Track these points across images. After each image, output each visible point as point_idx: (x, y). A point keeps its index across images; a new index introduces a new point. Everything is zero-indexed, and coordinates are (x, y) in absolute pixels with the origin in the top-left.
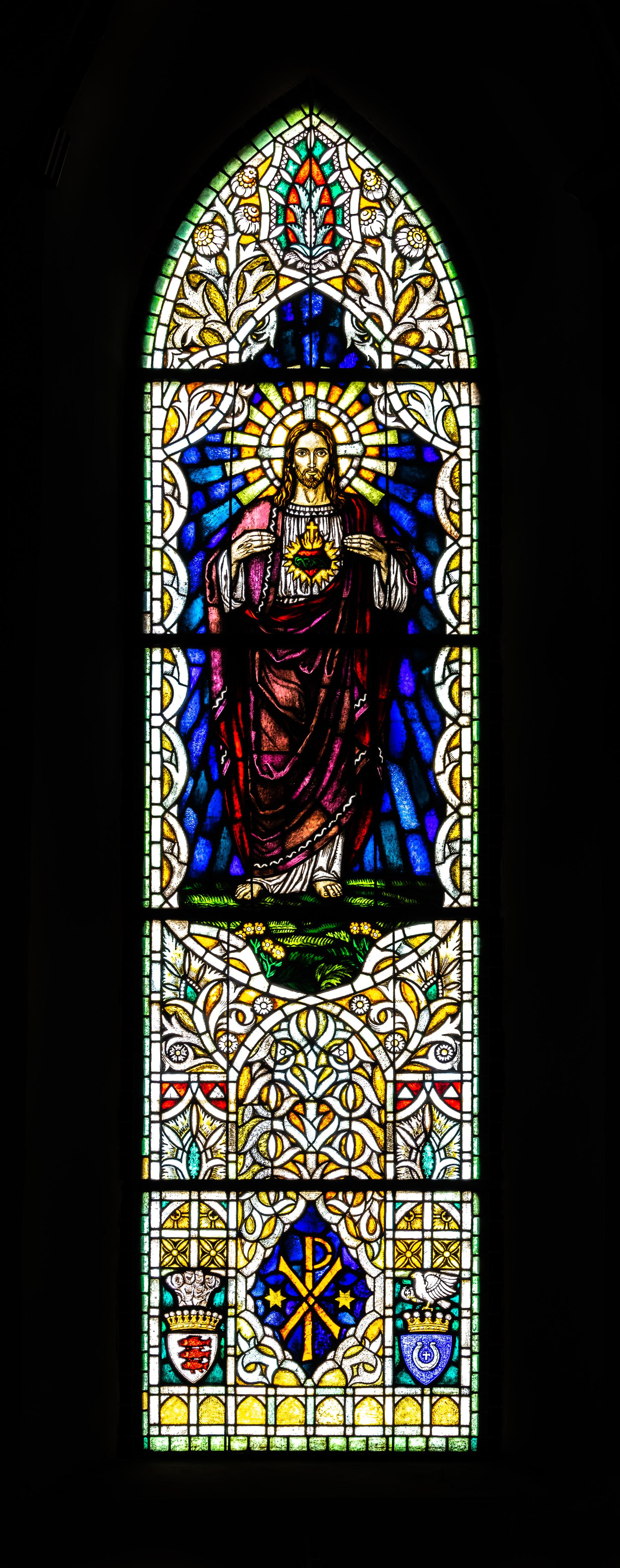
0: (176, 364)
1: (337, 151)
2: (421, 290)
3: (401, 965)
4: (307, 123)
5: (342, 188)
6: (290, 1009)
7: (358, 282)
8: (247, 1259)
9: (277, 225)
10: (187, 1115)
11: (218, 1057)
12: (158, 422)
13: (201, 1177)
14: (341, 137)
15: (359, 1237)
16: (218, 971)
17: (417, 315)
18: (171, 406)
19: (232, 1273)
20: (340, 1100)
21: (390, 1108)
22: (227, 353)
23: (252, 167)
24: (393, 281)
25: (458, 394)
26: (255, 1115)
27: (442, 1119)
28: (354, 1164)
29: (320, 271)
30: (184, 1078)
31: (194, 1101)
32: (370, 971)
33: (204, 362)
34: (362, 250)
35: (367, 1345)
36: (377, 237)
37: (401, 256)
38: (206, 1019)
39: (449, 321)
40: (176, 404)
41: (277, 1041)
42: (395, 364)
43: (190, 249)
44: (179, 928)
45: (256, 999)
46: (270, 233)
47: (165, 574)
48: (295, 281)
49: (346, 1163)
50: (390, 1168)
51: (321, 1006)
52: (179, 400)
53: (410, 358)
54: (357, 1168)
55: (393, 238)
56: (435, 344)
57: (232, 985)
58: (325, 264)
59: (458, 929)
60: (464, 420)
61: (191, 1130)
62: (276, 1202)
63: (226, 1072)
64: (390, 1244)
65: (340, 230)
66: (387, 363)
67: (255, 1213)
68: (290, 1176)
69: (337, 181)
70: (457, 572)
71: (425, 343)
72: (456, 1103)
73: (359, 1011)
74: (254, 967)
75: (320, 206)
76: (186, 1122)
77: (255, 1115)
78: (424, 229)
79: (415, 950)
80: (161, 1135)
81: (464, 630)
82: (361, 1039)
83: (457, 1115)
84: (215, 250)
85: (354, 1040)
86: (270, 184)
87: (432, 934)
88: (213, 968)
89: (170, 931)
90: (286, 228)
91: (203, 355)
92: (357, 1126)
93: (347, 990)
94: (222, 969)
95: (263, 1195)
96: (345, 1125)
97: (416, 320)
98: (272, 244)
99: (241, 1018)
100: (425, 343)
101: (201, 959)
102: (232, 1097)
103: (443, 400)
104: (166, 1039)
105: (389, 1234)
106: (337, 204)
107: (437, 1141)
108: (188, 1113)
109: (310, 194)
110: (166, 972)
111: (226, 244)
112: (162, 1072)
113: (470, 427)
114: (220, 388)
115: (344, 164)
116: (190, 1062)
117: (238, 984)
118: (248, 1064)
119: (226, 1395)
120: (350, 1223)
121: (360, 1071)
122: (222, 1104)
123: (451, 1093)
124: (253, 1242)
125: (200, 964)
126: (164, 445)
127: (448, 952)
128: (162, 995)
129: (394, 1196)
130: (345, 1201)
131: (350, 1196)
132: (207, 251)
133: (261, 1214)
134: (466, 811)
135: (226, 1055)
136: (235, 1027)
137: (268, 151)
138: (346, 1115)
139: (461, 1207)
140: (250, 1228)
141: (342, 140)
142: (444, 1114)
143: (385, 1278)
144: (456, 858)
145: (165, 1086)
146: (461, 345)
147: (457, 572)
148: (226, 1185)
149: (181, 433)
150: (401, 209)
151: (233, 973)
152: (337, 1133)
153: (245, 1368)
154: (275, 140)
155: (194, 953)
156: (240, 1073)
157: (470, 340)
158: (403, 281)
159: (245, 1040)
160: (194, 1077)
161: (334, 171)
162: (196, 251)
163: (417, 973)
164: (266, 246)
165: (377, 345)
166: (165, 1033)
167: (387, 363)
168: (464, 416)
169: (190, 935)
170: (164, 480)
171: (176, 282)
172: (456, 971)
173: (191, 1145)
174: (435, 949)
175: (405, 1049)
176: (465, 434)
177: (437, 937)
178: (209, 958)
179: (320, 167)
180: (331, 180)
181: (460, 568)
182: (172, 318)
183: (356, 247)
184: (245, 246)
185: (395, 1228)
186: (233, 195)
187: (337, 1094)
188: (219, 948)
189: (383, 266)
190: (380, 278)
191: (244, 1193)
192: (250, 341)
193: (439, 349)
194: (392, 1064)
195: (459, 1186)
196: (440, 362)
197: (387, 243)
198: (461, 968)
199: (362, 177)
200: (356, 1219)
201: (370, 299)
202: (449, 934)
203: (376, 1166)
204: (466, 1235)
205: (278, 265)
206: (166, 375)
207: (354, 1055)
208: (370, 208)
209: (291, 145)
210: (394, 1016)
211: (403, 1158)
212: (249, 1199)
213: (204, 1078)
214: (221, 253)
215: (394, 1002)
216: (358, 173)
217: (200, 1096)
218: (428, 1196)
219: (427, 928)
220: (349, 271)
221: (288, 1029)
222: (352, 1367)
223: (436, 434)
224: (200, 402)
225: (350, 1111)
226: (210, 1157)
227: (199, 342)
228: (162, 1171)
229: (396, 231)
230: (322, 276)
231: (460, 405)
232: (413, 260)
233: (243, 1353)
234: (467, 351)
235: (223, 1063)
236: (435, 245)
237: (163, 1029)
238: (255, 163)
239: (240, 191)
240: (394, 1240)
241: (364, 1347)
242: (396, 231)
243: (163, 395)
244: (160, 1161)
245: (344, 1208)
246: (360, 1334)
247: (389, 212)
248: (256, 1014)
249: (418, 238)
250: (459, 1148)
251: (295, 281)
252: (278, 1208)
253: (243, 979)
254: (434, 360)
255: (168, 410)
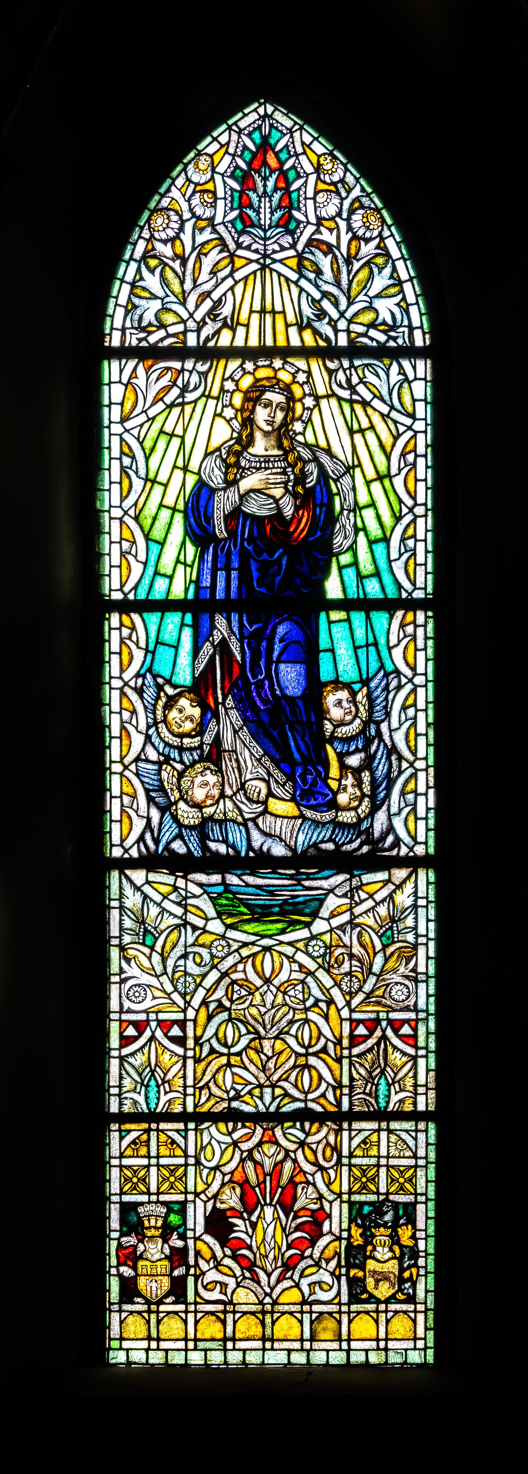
0: (134, 343)
1: (292, 137)
2: (376, 270)
3: (358, 910)
4: (261, 111)
5: (281, 132)
6: (245, 952)
7: (314, 263)
8: (206, 1183)
9: (232, 209)
10: (146, 1051)
11: (176, 997)
12: (117, 397)
13: (158, 1110)
14: (296, 123)
15: (316, 1164)
16: (175, 916)
17: (372, 293)
18: (129, 382)
19: (190, 1197)
20: (296, 1037)
21: (345, 1043)
22: (185, 333)
23: (206, 154)
24: (348, 262)
25: (414, 368)
26: (212, 1051)
27: (398, 1055)
28: (311, 1096)
29: (274, 252)
30: (143, 1017)
31: (153, 1038)
32: (326, 916)
33: (162, 340)
34: (318, 231)
35: (324, 1265)
36: (332, 219)
37: (355, 237)
38: (164, 960)
39: (404, 299)
40: (134, 381)
41: (233, 982)
42: (350, 341)
43: (146, 234)
44: (138, 876)
45: (212, 943)
46: (225, 216)
47: (123, 542)
48: (250, 261)
49: (302, 1096)
50: (345, 1101)
51: (276, 948)
52: (136, 377)
53: (365, 335)
54: (313, 1100)
55: (348, 220)
56: (390, 321)
57: (189, 928)
58: (280, 245)
59: (413, 879)
60: (419, 394)
61: (150, 1065)
62: (235, 1129)
63: (184, 1011)
64: (345, 1170)
65: (295, 213)
66: (343, 341)
67: (213, 1142)
68: (247, 1109)
69: (293, 167)
70: (413, 540)
71: (380, 320)
72: (412, 1040)
73: (316, 954)
74: (211, 912)
75: (276, 189)
76: (145, 1058)
77: (212, 1051)
78: (378, 210)
79: (371, 896)
80: (120, 1069)
81: (419, 594)
82: (316, 979)
83: (411, 1051)
84: (171, 233)
85: (309, 979)
86: (226, 172)
87: (389, 881)
88: (171, 914)
89: (128, 879)
90: (242, 212)
91: (162, 333)
92: (313, 1061)
93: (304, 933)
94: (180, 915)
95: (222, 1126)
96: (302, 1061)
97: (371, 298)
98: (226, 227)
99: (198, 960)
100: (380, 320)
101: (159, 905)
102: (190, 1033)
103: (399, 373)
104: (123, 981)
105: (345, 1161)
106: (293, 188)
107: (392, 1075)
108: (147, 1048)
109: (265, 179)
110: (125, 917)
111: (181, 229)
112: (121, 1012)
113: (425, 400)
114: (177, 365)
115: (299, 150)
116: (148, 1004)
117: (195, 928)
118: (204, 1003)
119: (186, 1312)
120: (308, 1152)
121: (316, 1010)
122: (181, 1041)
123: (406, 1030)
124: (211, 1169)
125: (158, 910)
126: (123, 420)
127: (403, 899)
128: (121, 940)
129: (350, 1125)
130: (303, 1129)
131: (307, 1125)
132: (163, 236)
133: (219, 1142)
134: (420, 765)
135: (183, 996)
136: (192, 968)
137: (224, 139)
138: (303, 1051)
139: (416, 1026)
140: (209, 1155)
141: (297, 127)
142: (398, 1050)
143: (342, 1202)
144: (412, 818)
145: (124, 1025)
146: (416, 323)
147: (413, 540)
148: (184, 1117)
149: (138, 410)
150: (356, 192)
151: (191, 918)
152: (295, 1067)
153: (205, 1287)
154: (230, 128)
155: (151, 900)
156: (197, 1011)
157: (424, 318)
158: (358, 260)
159: (202, 981)
160: (153, 1016)
161: (291, 157)
162: (152, 236)
163: (372, 919)
164: (221, 229)
165: (333, 324)
166: (123, 976)
167: (343, 341)
168: (419, 389)
169: (148, 882)
170: (122, 452)
171: (133, 266)
172: (412, 916)
173: (150, 1080)
174: (391, 896)
175: (360, 989)
176: (420, 407)
177: (394, 884)
178: (166, 904)
179: (277, 154)
180: (287, 166)
181: (414, 536)
182: (129, 300)
183: (311, 229)
184: (202, 230)
185: (351, 1155)
186: (189, 180)
187: (293, 1031)
188: (175, 894)
189: (338, 248)
190: (335, 257)
191: (202, 1123)
192: (207, 320)
193: (394, 327)
194: (348, 1004)
195: (415, 1116)
196: (395, 339)
197: (343, 225)
198: (416, 913)
199: (318, 161)
200: (314, 1146)
201: (324, 278)
202: (404, 882)
203: (331, 1099)
204: (421, 1162)
205: (232, 246)
206: (124, 353)
207: (310, 994)
208: (326, 191)
209: (246, 132)
210: (350, 960)
211: (359, 1091)
212: (208, 1128)
213: (162, 1016)
214: (177, 237)
215: (351, 947)
216: (314, 159)
217: (159, 1034)
218: (384, 1125)
219: (383, 876)
220: (303, 252)
221: (244, 971)
222: (309, 1285)
223: (392, 407)
224: (158, 379)
225: (307, 1048)
226: (168, 1090)
227: (155, 323)
228: (121, 1104)
229: (352, 211)
230: (277, 256)
231: (416, 379)
232: (367, 241)
233: (203, 1273)
234: (421, 327)
235: (181, 1003)
236: (389, 227)
237: (122, 971)
238: (210, 150)
239: (195, 178)
240: (350, 1165)
241: (320, 1267)
242: (352, 211)
243: (121, 371)
244: (119, 1095)
245: (302, 1136)
246: (317, 1255)
247: (344, 194)
248: (213, 957)
249: (374, 221)
250: (415, 1075)
251: (250, 261)
252: (236, 1136)
253: (200, 923)
254: (390, 338)
255: (126, 386)
